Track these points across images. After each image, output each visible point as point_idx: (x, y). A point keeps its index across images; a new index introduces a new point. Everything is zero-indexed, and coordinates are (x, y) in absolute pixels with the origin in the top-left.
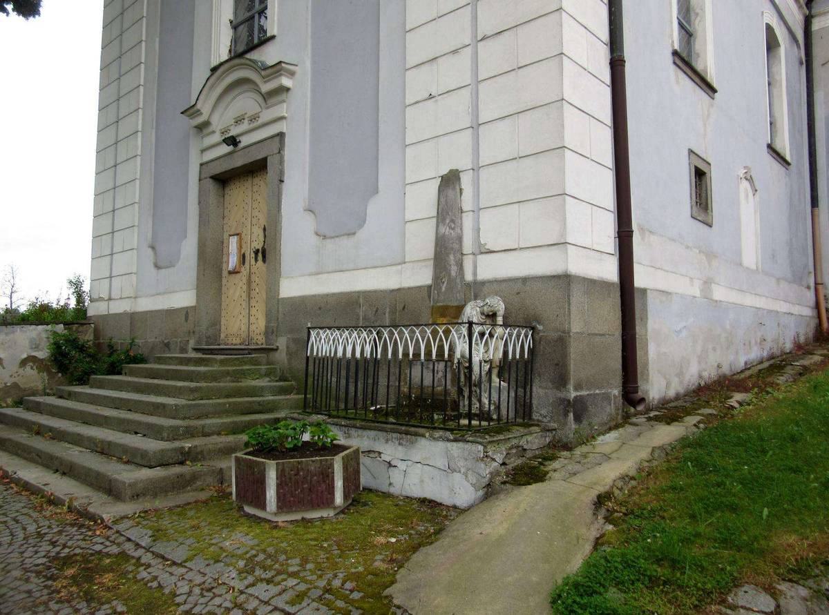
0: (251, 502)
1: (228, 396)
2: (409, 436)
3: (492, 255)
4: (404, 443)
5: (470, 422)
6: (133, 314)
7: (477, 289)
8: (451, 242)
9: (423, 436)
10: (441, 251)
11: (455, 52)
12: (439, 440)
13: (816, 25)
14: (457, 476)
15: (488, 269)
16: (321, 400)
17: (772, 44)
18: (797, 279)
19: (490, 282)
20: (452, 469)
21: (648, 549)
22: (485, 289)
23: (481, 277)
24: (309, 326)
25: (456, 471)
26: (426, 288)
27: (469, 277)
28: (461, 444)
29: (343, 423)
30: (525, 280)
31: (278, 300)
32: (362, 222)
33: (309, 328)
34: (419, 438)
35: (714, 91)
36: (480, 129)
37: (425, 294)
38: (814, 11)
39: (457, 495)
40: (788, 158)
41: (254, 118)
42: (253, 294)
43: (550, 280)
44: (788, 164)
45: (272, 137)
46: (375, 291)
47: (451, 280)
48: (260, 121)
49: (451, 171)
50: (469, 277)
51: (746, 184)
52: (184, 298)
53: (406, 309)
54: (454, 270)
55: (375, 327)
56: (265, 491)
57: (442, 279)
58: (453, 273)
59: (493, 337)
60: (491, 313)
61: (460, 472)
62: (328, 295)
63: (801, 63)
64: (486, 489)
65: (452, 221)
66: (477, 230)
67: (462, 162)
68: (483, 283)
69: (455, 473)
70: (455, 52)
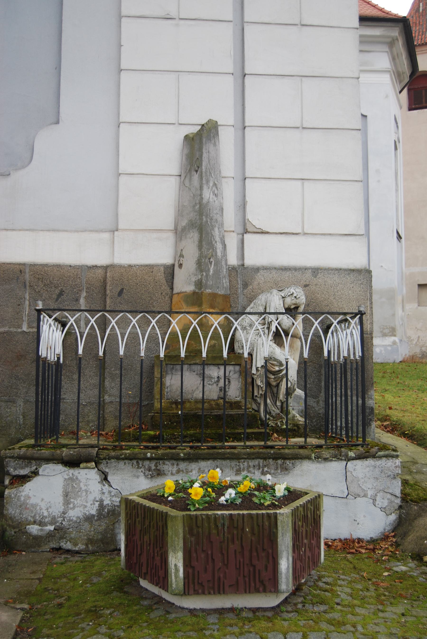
0: (145, 574)
2: (280, 462)
3: (267, 235)
4: (272, 471)
5: (306, 440)
8: (215, 212)
9: (308, 458)
10: (207, 222)
12: (331, 461)
16: (357, 386)
22: (260, 277)
24: (40, 306)
25: (359, 496)
26: (162, 269)
28: (370, 462)
29: (149, 455)
33: (39, 311)
34: (297, 462)
36: (121, 73)
37: (161, 276)
39: (360, 526)
43: (349, 274)
46: (59, 266)
49: (210, 121)
53: (124, 295)
55: (154, 312)
56: (167, 554)
57: (210, 259)
58: (219, 254)
59: (288, 335)
60: (293, 307)
61: (365, 496)
62: (4, 264)
64: (398, 512)
65: (215, 185)
68: (257, 270)
69: (358, 499)
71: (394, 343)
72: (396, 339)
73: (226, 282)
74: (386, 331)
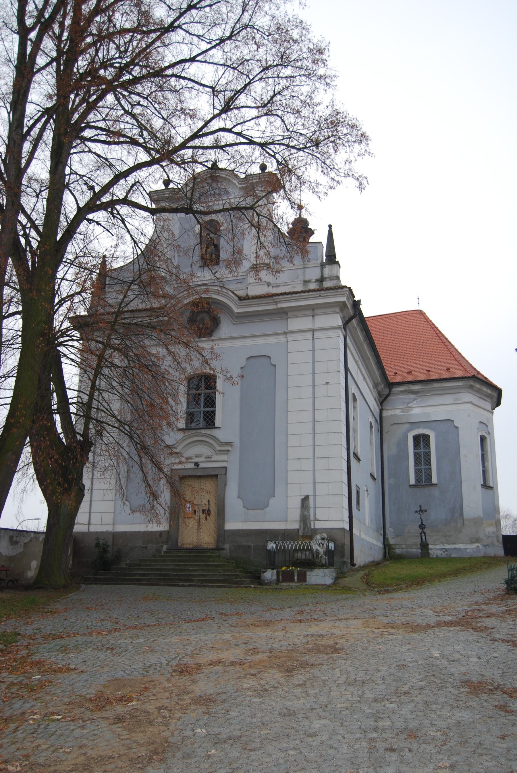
1: (188, 569)
6: (113, 533)
7: (316, 531)
11: (307, 459)
13: (385, 414)
14: (327, 577)
15: (319, 525)
17: (371, 427)
18: (377, 531)
19: (320, 529)
20: (325, 576)
21: (304, 669)
23: (317, 527)
27: (312, 527)
30: (331, 529)
31: (224, 530)
32: (267, 505)
35: (360, 460)
38: (384, 408)
40: (375, 477)
41: (210, 457)
42: (201, 527)
44: (375, 479)
45: (221, 467)
47: (308, 528)
48: (212, 459)
50: (312, 527)
51: (366, 492)
52: (163, 527)
54: (309, 525)
63: (378, 431)
66: (315, 514)
67: (310, 493)
68: (318, 529)
70: (307, 459)
71: (478, 547)
72: (479, 544)
73: (310, 532)
74: (473, 540)
